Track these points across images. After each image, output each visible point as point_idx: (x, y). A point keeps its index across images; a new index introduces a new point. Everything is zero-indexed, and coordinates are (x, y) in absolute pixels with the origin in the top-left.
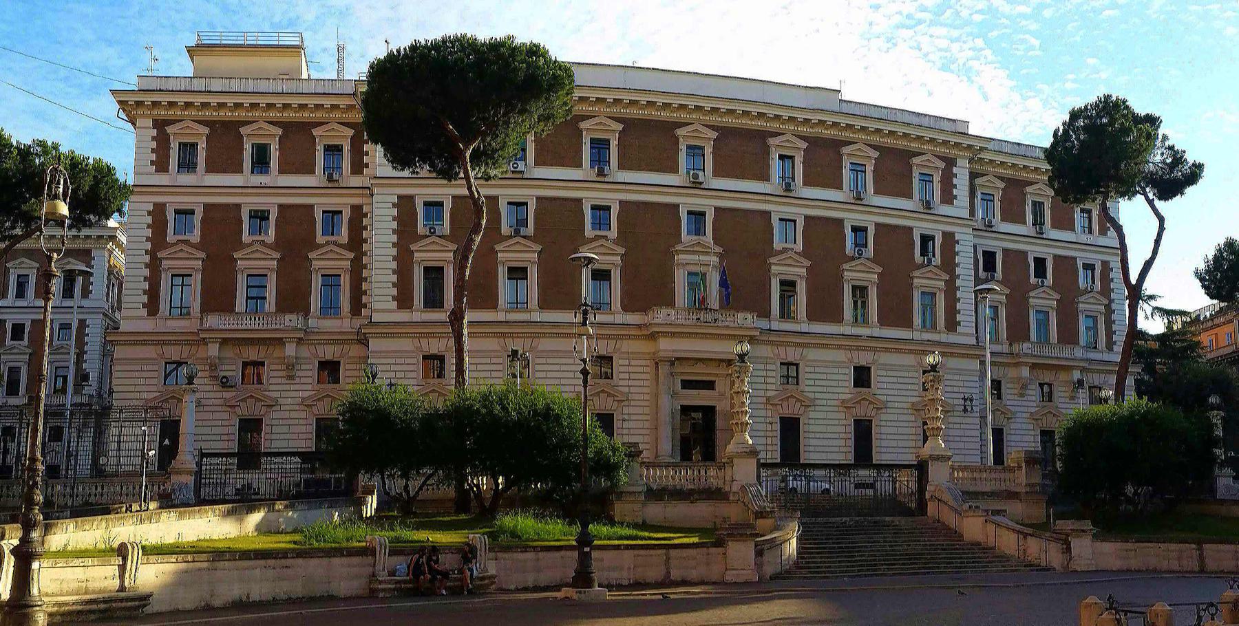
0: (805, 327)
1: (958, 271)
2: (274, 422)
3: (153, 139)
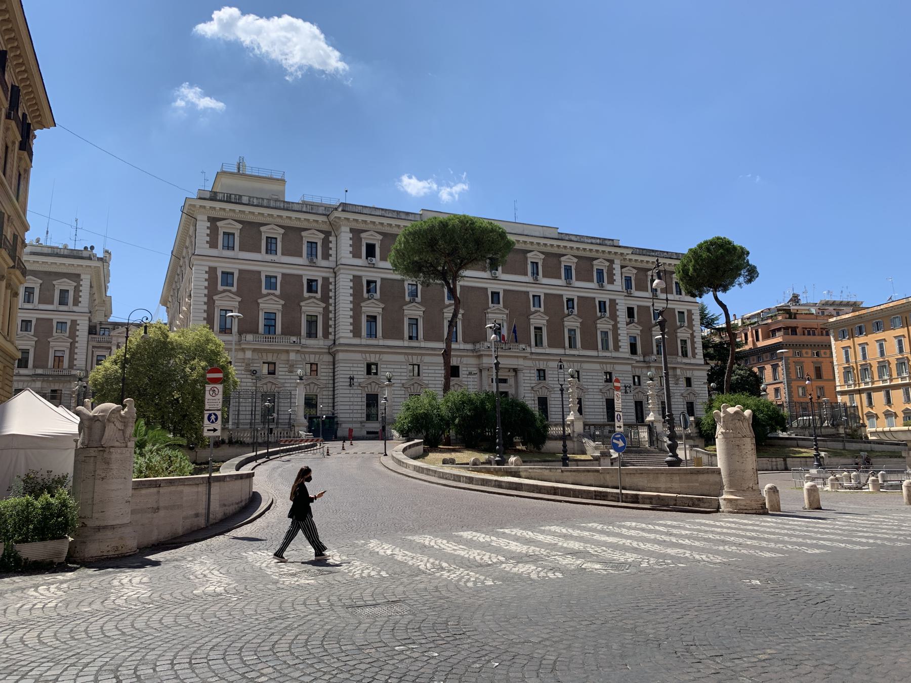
0: (381, 342)
1: (619, 319)
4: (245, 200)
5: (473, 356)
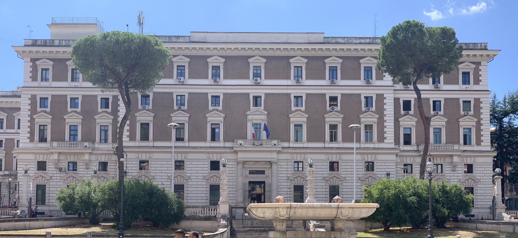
0: (306, 145)
2: (189, 186)
3: (31, 67)
4: (56, 43)
5: (231, 153)
